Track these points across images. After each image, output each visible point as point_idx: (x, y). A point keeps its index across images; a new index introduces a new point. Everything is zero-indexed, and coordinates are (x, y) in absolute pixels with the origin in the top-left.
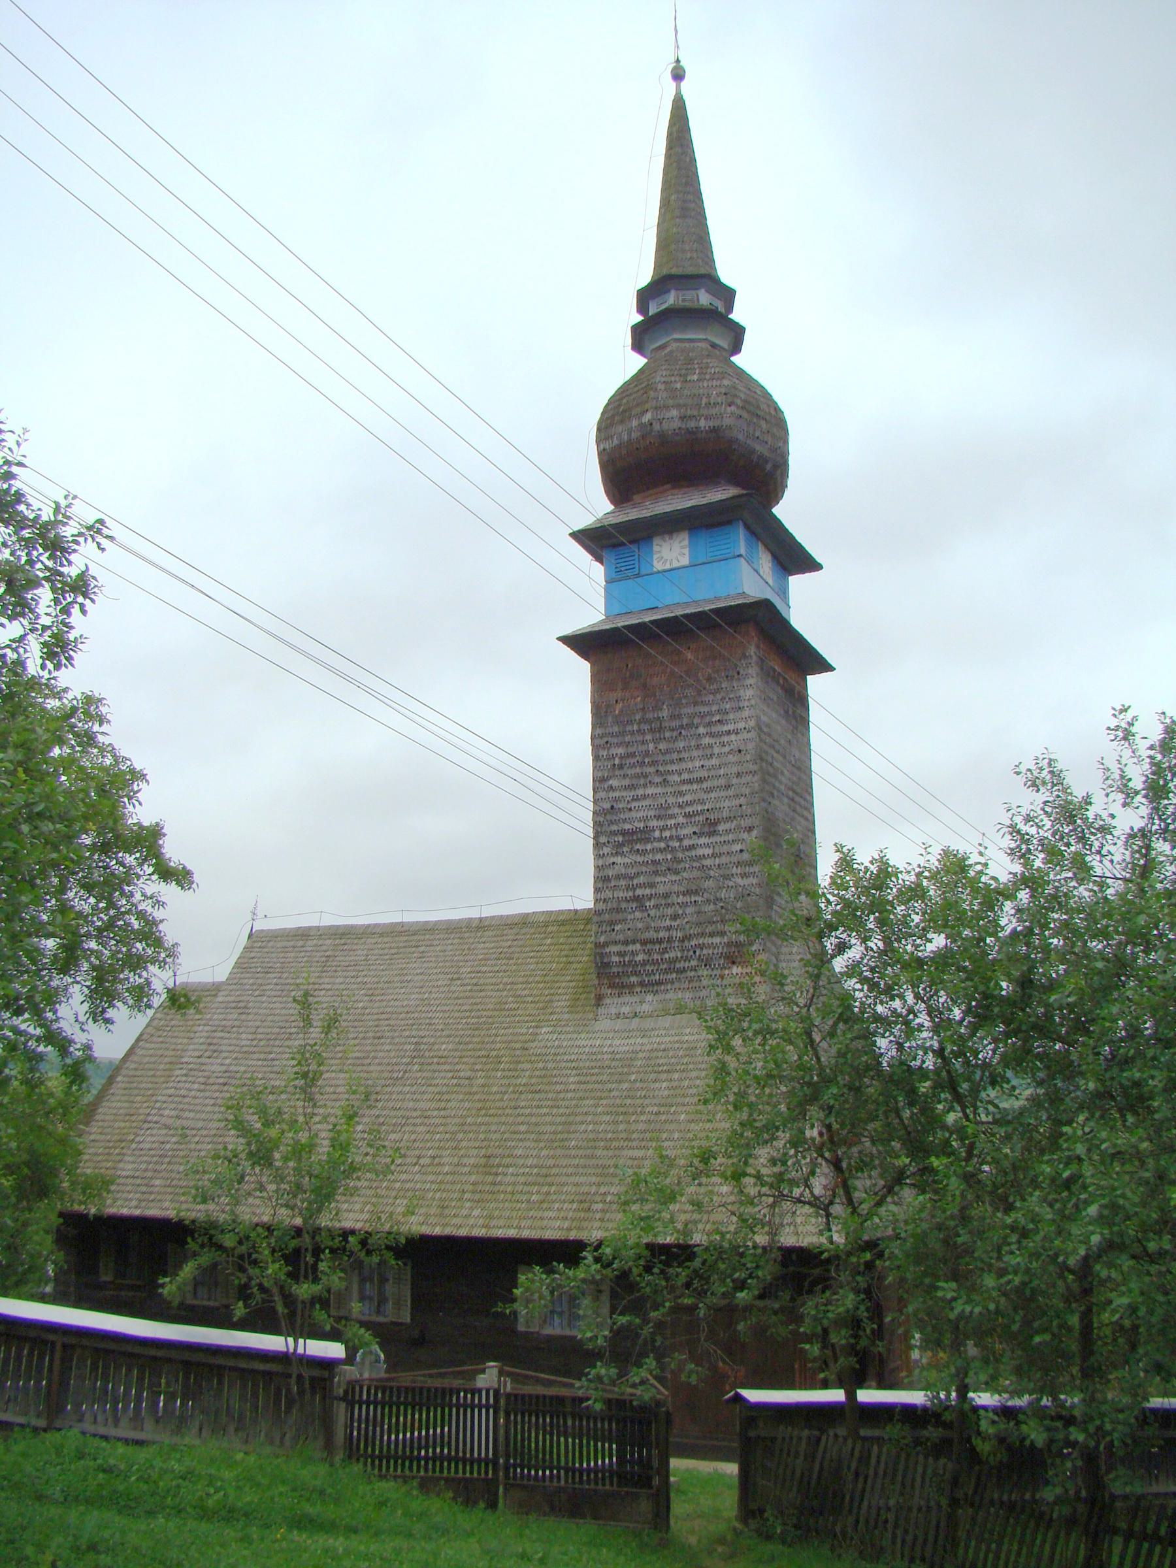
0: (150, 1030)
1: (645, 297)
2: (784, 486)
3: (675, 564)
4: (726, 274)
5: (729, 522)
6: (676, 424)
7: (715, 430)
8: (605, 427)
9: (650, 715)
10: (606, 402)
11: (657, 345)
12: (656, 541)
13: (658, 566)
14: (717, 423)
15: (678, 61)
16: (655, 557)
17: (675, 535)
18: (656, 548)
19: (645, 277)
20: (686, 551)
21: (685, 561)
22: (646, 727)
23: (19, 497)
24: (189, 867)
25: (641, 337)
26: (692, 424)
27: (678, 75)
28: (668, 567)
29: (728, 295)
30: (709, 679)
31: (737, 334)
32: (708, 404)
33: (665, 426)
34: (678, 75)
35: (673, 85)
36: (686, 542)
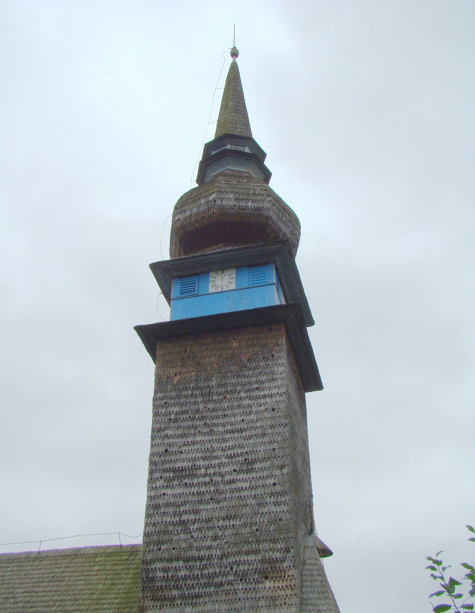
3: (225, 289)
5: (266, 264)
6: (232, 202)
7: (257, 209)
9: (201, 384)
11: (231, 168)
12: (212, 274)
13: (211, 290)
14: (259, 205)
18: (211, 279)
20: (234, 281)
21: (233, 287)
22: (197, 392)
26: (243, 204)
28: (219, 290)
30: (249, 360)
32: (254, 194)
33: (224, 203)
36: (234, 276)
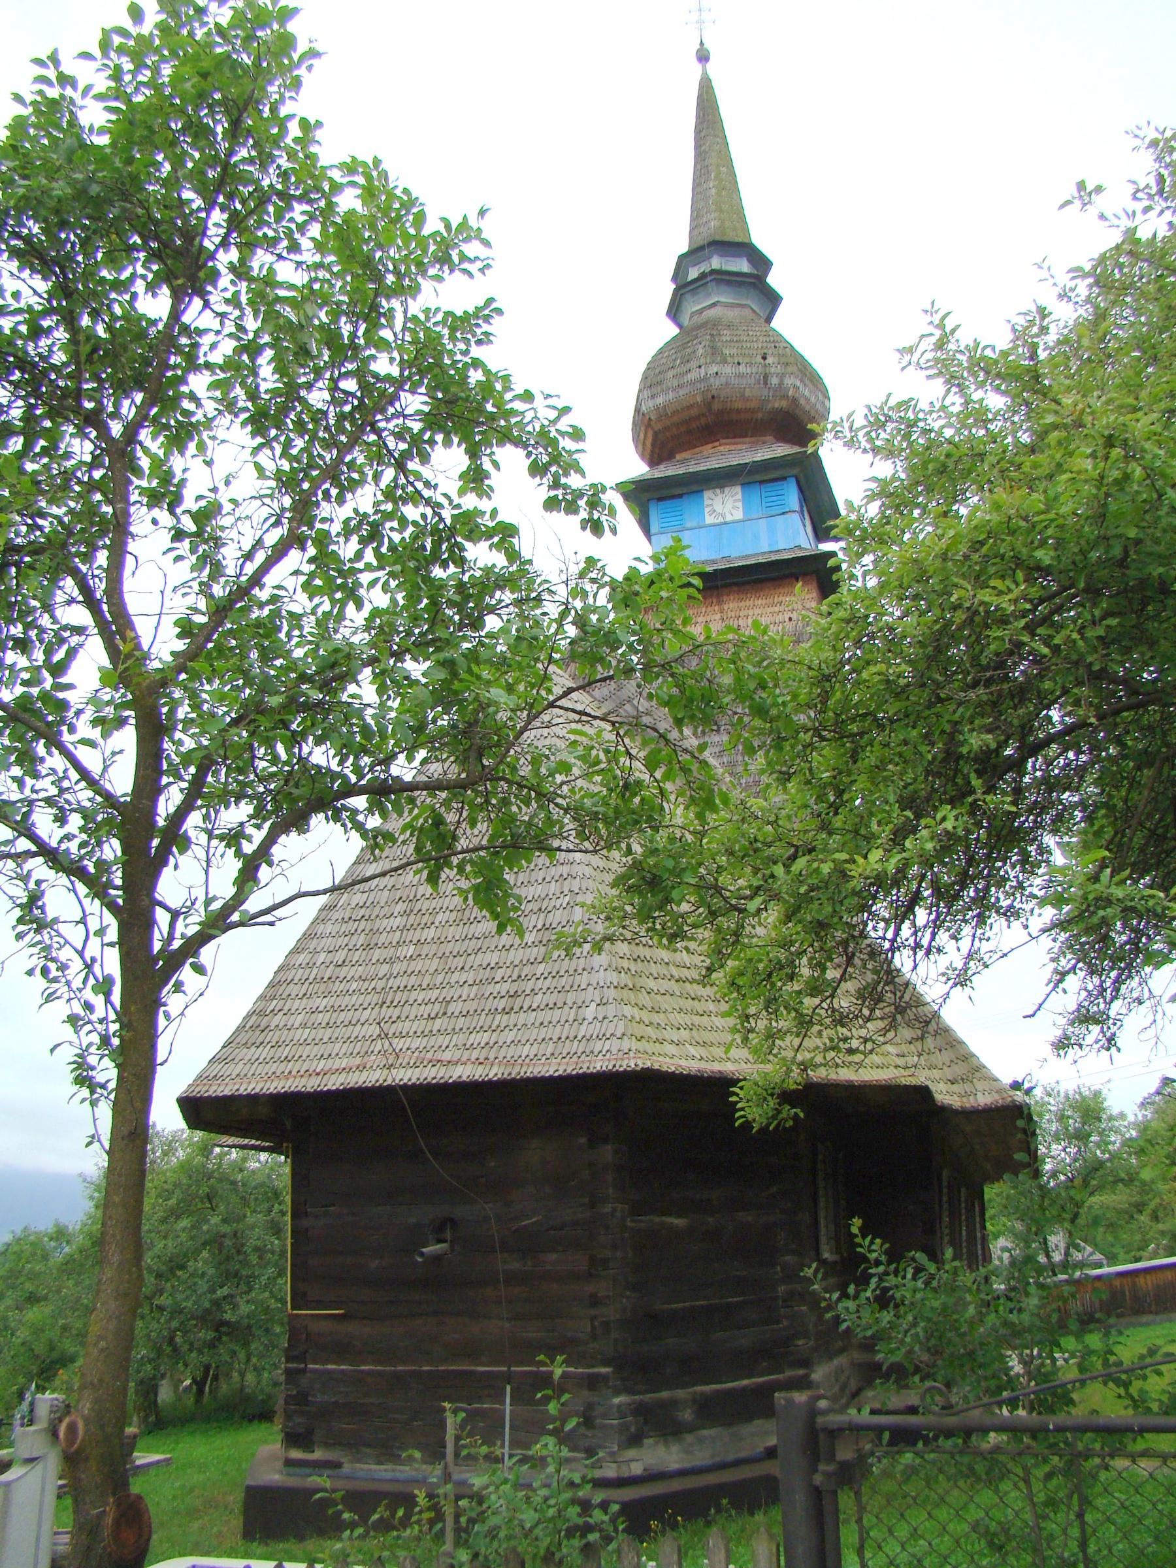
0: (302, 958)
1: (683, 262)
2: (636, 439)
3: (729, 518)
4: (760, 239)
5: (783, 479)
8: (652, 379)
10: (644, 367)
12: (707, 494)
13: (709, 520)
15: (702, 43)
16: (707, 510)
17: (727, 490)
18: (707, 502)
19: (683, 246)
20: (740, 505)
21: (739, 515)
23: (227, 808)
24: (8, 121)
25: (674, 311)
27: (703, 57)
28: (720, 520)
29: (762, 263)
31: (772, 299)
34: (703, 57)
35: (699, 67)
36: (739, 496)
